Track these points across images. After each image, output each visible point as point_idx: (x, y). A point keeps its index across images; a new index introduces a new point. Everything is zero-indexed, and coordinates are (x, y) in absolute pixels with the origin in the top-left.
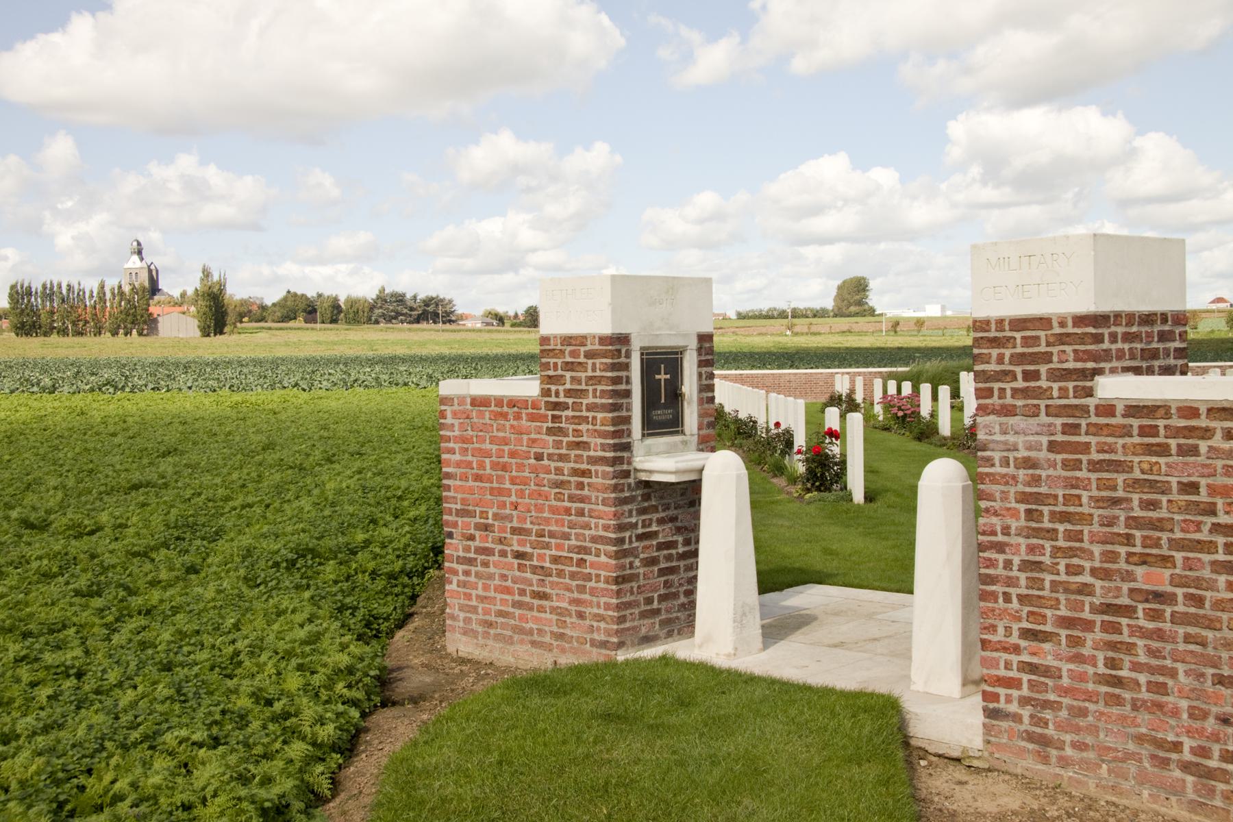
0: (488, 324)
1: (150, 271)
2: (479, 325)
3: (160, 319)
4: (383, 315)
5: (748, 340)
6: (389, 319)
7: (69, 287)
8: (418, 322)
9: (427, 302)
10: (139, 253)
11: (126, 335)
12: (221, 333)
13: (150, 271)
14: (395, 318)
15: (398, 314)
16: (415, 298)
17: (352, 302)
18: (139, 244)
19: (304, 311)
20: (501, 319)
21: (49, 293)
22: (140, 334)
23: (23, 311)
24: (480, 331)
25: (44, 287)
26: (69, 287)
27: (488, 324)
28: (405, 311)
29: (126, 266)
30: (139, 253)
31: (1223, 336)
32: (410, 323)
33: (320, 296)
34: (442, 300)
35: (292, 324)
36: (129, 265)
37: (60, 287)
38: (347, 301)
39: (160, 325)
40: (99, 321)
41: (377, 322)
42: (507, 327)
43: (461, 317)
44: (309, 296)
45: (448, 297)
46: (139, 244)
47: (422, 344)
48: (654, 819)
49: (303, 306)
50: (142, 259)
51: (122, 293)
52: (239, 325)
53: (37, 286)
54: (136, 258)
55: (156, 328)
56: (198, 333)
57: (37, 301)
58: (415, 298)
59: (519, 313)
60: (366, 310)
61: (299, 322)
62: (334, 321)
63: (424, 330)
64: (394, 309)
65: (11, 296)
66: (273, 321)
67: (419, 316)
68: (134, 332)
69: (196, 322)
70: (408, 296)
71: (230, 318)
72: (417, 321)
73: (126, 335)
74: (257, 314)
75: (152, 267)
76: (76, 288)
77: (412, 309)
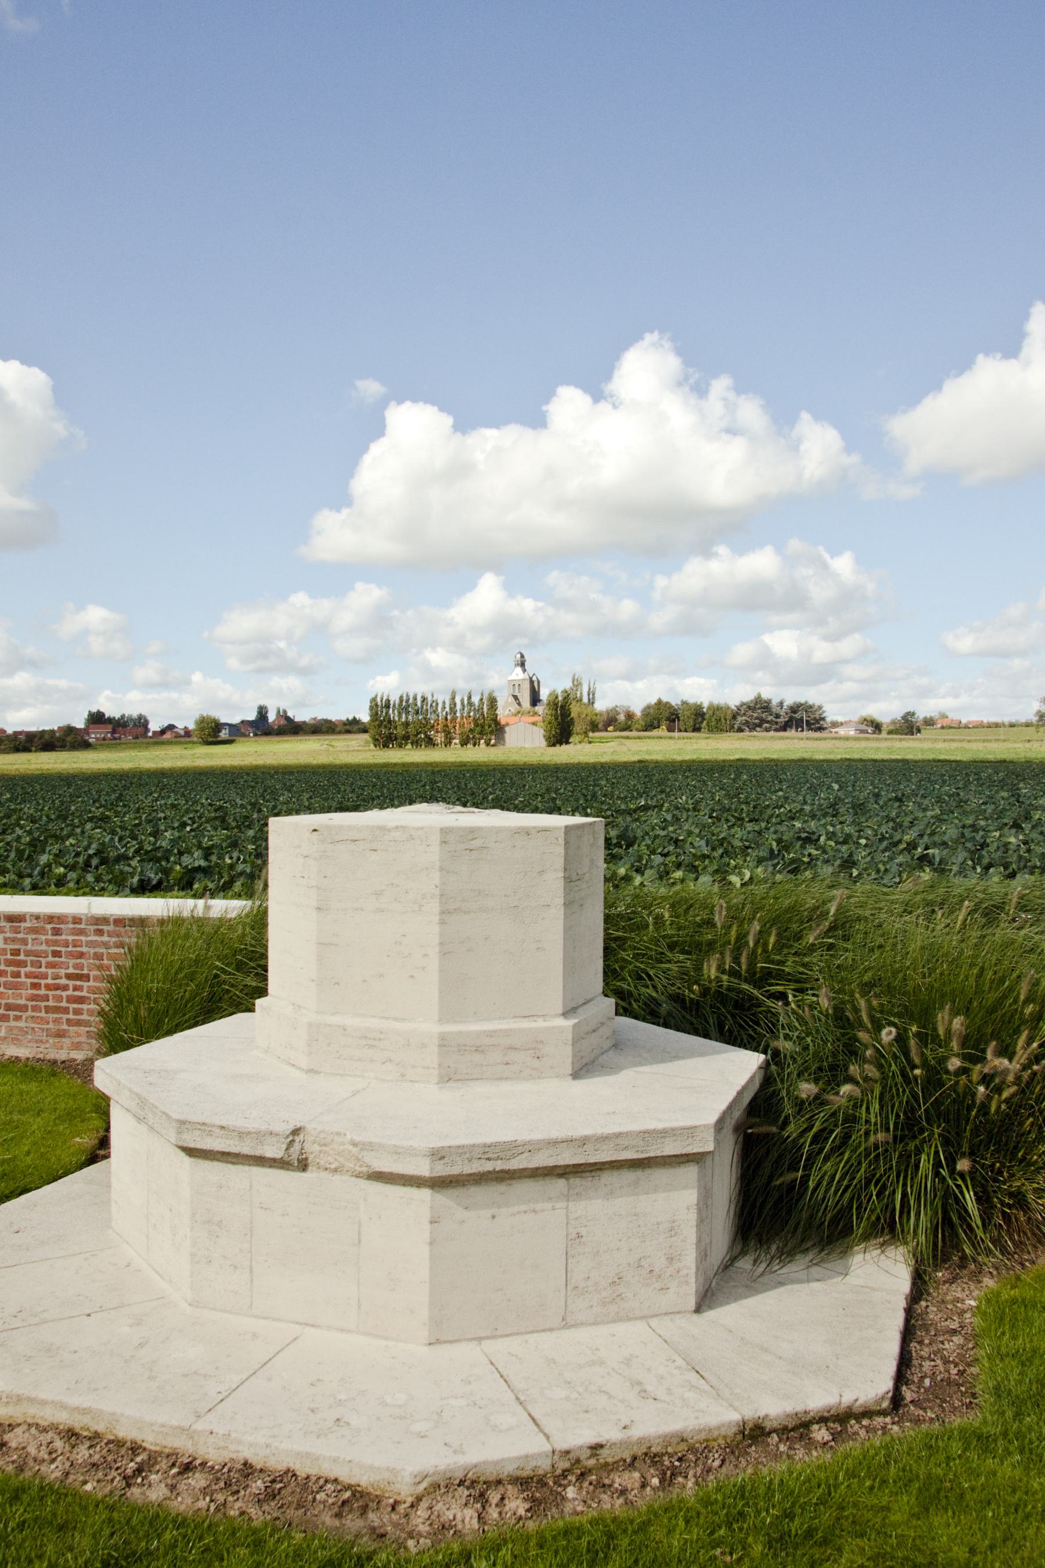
0: (862, 731)
1: (532, 682)
2: (852, 733)
3: (507, 729)
4: (747, 723)
5: (974, 746)
6: (753, 727)
7: (424, 699)
8: (785, 730)
9: (794, 709)
10: (522, 664)
11: (474, 745)
12: (567, 743)
13: (532, 682)
14: (760, 726)
15: (763, 721)
16: (781, 704)
17: (716, 709)
18: (522, 656)
19: (668, 719)
20: (877, 727)
21: (405, 705)
22: (488, 744)
23: (382, 722)
24: (856, 739)
25: (401, 698)
26: (424, 699)
27: (862, 731)
28: (770, 718)
29: (510, 678)
30: (522, 664)
31: (533, 758)
32: (776, 730)
33: (684, 703)
34: (811, 707)
35: (655, 733)
36: (513, 677)
37: (415, 699)
38: (709, 708)
39: (507, 736)
40: (449, 733)
41: (740, 730)
42: (884, 735)
43: (835, 724)
44: (673, 704)
45: (817, 704)
46: (522, 656)
47: (648, 752)
48: (1043, 1385)
49: (667, 714)
50: (524, 671)
51: (470, 704)
52: (591, 734)
53: (394, 698)
54: (519, 669)
55: (503, 739)
56: (544, 743)
57: (393, 714)
58: (781, 704)
59: (785, 704)
60: (729, 717)
61: (662, 731)
62: (697, 729)
63: (793, 738)
64: (759, 716)
65: (371, 708)
66: (638, 730)
67: (786, 723)
68: (482, 741)
69: (542, 732)
70: (774, 702)
71: (577, 728)
72: (784, 728)
73: (474, 745)
74: (614, 722)
75: (534, 678)
76: (430, 699)
77: (778, 716)
